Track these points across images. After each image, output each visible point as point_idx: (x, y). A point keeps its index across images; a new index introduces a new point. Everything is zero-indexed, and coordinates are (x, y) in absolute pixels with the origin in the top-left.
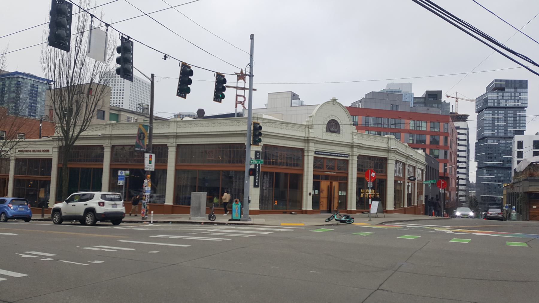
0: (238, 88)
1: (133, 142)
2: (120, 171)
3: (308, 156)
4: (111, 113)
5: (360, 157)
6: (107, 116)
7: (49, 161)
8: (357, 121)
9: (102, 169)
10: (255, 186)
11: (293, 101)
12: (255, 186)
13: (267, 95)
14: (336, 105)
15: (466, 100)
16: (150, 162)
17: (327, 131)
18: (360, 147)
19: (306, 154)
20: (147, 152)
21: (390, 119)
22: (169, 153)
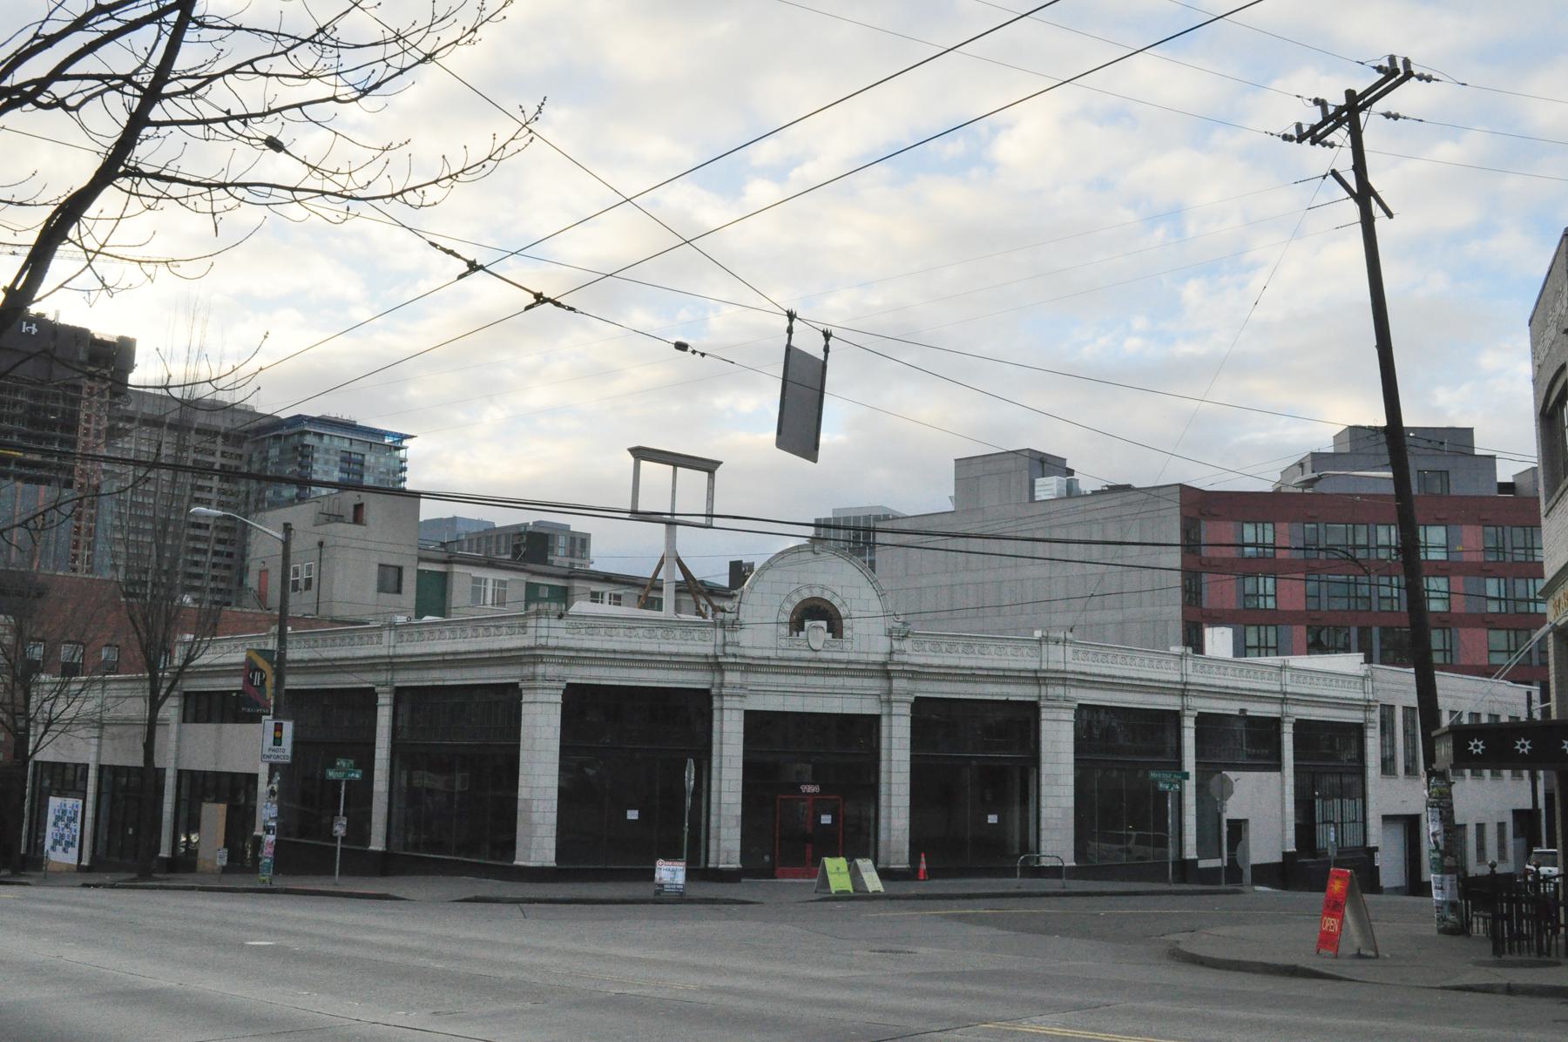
1: (236, 683)
3: (722, 709)
4: (420, 572)
5: (921, 706)
6: (668, 596)
15: (1340, 979)
18: (915, 674)
19: (716, 704)
22: (524, 707)
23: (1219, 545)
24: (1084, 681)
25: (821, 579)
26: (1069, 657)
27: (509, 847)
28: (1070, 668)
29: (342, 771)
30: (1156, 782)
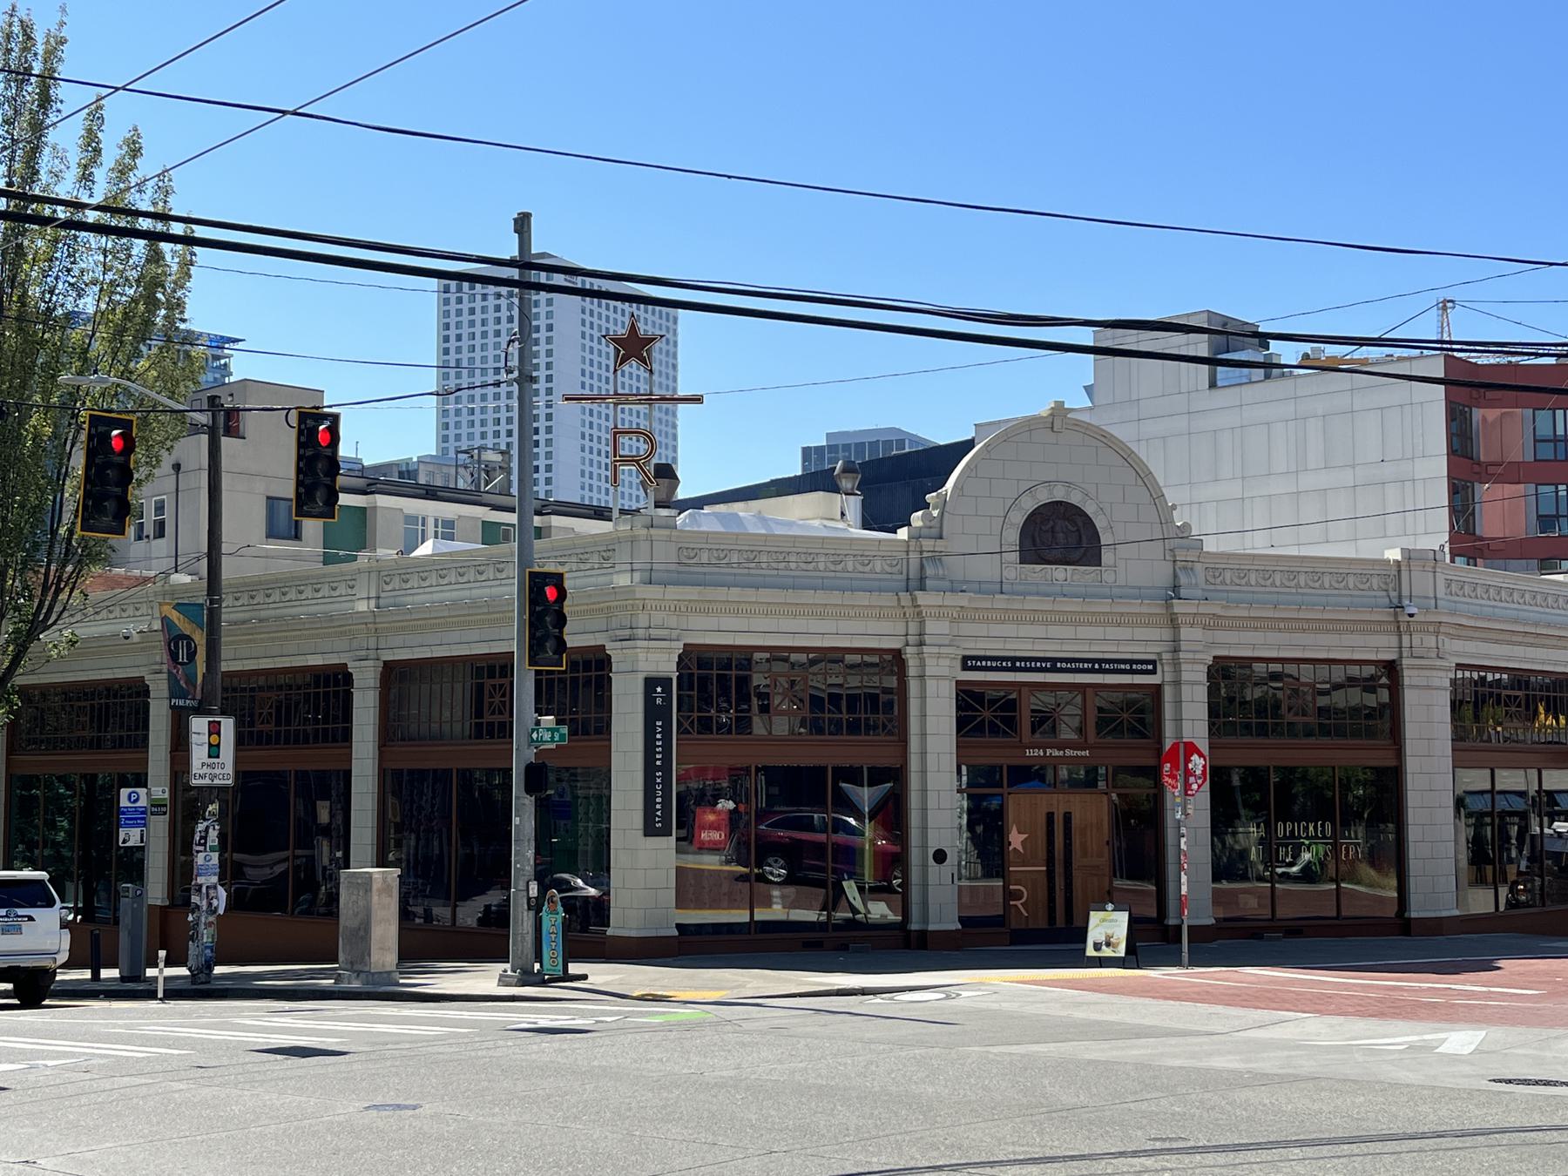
0: (620, 399)
2: (124, 792)
7: (137, 691)
10: (650, 830)
12: (650, 830)
16: (214, 750)
20: (200, 711)
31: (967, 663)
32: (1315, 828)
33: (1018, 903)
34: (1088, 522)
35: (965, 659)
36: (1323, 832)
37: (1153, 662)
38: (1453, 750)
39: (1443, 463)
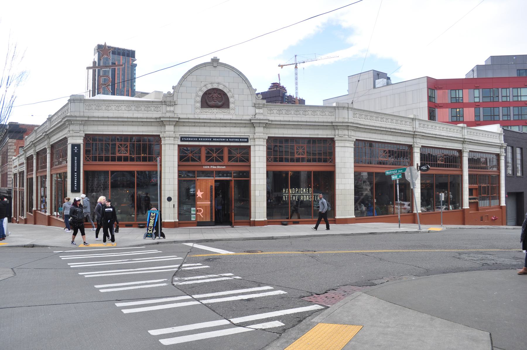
8: (461, 96)
9: (469, 183)
11: (377, 81)
13: (347, 78)
14: (220, 68)
17: (202, 106)
18: (267, 125)
21: (511, 89)
23: (443, 96)
24: (358, 128)
25: (220, 80)
26: (417, 126)
27: (249, 215)
28: (350, 121)
29: (225, 175)
30: (390, 176)
31: (182, 139)
32: (306, 190)
33: (200, 214)
34: (225, 94)
35: (181, 138)
36: (308, 191)
37: (247, 139)
38: (267, 165)
39: (427, 103)
